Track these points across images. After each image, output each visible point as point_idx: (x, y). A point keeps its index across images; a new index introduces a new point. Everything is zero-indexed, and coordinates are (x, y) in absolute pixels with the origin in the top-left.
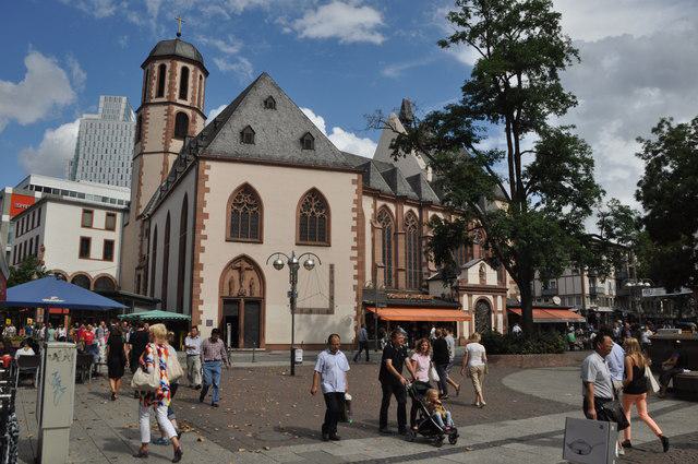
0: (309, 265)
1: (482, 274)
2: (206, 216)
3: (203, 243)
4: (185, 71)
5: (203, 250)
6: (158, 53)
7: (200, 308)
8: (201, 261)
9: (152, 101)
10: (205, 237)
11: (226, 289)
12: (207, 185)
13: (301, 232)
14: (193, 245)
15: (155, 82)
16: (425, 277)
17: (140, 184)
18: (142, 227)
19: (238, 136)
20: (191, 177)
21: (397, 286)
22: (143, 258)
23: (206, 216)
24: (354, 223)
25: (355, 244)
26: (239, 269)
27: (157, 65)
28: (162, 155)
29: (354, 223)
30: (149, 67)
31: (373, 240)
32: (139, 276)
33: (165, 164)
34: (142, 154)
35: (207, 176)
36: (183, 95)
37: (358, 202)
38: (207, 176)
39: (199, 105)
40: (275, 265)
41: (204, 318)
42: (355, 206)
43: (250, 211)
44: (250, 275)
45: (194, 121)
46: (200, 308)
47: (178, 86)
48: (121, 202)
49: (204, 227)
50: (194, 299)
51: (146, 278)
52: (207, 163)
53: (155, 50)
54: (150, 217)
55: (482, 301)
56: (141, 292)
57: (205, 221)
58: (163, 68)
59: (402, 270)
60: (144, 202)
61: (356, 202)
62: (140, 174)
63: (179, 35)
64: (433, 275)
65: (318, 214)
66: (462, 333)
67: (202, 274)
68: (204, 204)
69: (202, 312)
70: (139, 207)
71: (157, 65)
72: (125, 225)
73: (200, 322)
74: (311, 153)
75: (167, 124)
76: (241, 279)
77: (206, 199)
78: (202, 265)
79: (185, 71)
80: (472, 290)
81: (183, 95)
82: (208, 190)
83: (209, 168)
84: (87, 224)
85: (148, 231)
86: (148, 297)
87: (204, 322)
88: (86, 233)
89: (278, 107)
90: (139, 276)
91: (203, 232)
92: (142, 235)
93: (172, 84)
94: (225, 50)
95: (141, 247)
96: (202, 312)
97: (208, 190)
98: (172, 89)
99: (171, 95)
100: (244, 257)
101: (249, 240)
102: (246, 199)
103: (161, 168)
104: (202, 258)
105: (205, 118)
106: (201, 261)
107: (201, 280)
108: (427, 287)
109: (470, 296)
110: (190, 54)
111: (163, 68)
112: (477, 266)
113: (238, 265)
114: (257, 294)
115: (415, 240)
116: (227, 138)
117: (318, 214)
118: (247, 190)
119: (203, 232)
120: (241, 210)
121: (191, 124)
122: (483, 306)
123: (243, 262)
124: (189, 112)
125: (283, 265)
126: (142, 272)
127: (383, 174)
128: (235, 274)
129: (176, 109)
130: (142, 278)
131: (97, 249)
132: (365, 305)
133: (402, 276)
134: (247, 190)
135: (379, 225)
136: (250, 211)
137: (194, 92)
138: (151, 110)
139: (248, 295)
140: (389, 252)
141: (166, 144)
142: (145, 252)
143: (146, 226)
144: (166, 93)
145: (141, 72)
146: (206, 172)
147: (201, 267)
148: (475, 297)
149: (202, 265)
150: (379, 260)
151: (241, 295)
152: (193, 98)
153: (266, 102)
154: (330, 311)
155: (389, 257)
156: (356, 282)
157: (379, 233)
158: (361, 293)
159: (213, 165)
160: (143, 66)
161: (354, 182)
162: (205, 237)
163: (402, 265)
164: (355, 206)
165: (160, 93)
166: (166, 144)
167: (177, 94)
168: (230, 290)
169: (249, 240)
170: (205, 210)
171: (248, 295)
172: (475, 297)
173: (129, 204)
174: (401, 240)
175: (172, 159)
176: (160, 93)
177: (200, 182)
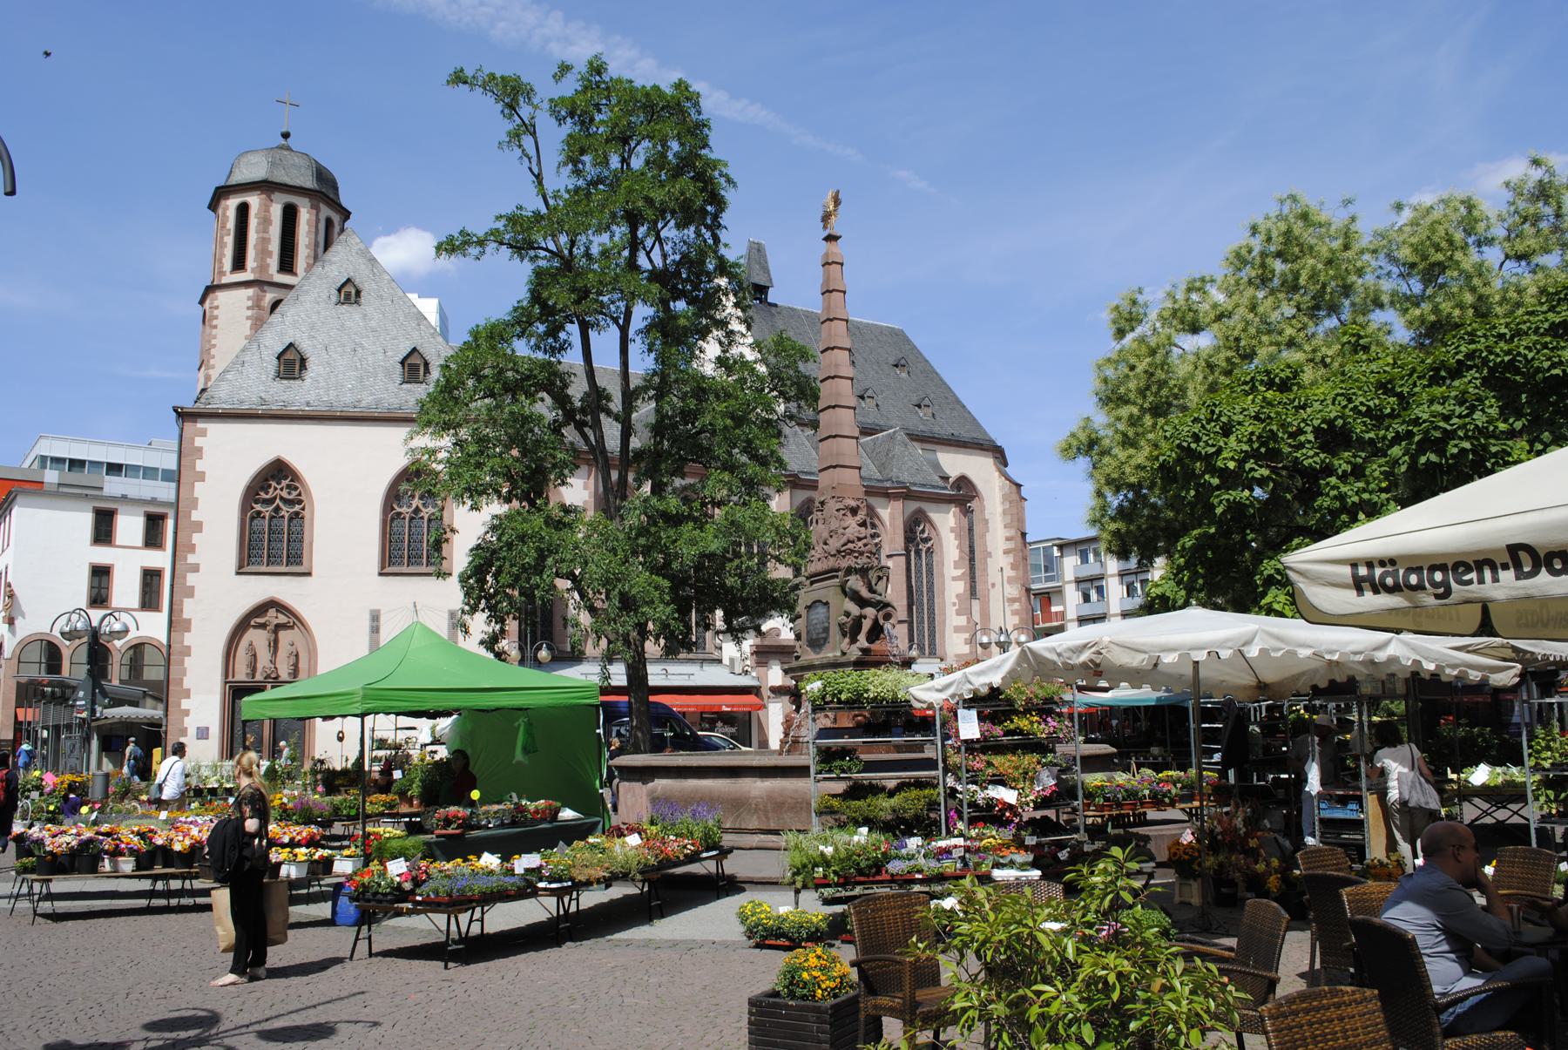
2: (198, 527)
5: (190, 592)
7: (185, 704)
8: (185, 615)
9: (225, 280)
10: (195, 568)
23: (198, 527)
27: (232, 203)
35: (200, 450)
38: (200, 450)
41: (191, 724)
43: (286, 511)
47: (275, 246)
49: (192, 548)
52: (200, 425)
57: (196, 538)
58: (243, 210)
68: (194, 503)
69: (187, 713)
71: (232, 203)
76: (274, 645)
78: (189, 622)
83: (203, 433)
84: (103, 530)
88: (102, 555)
91: (191, 559)
93: (264, 241)
96: (187, 713)
97: (201, 477)
98: (265, 222)
99: (263, 267)
100: (272, 604)
106: (185, 615)
107: (187, 651)
111: (243, 210)
117: (426, 512)
118: (278, 471)
119: (191, 559)
131: (125, 590)
134: (278, 471)
138: (222, 297)
146: (198, 442)
149: (189, 622)
159: (215, 429)
162: (195, 568)
165: (239, 263)
167: (274, 262)
169: (283, 569)
170: (195, 516)
176: (239, 263)
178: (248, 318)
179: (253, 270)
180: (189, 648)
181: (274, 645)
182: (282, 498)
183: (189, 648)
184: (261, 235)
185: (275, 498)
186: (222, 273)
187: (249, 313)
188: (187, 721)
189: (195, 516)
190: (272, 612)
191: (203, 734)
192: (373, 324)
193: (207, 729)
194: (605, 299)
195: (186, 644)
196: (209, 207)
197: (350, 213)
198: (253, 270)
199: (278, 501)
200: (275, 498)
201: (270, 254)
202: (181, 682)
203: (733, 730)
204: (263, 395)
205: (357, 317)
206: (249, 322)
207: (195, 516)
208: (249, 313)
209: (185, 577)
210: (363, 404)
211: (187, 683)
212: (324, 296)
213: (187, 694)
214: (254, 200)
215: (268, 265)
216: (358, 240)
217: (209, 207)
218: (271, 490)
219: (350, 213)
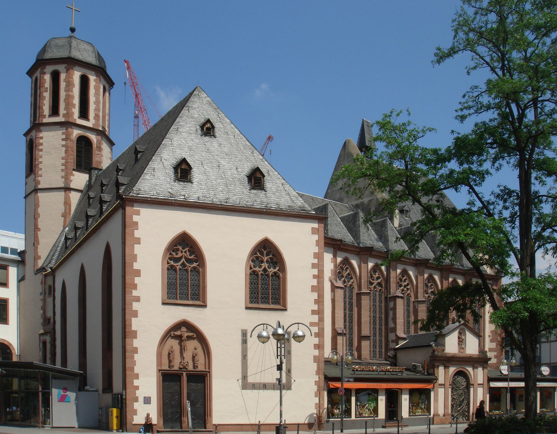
0: (299, 336)
1: (461, 341)
3: (136, 306)
4: (84, 81)
6: (48, 56)
7: (136, 383)
8: (134, 328)
9: (45, 120)
10: (138, 299)
11: (165, 361)
12: (137, 234)
13: (251, 293)
14: (124, 310)
15: (47, 96)
16: (392, 345)
17: (36, 228)
18: (44, 283)
19: (171, 172)
20: (116, 221)
21: (359, 357)
22: (47, 321)
24: (315, 282)
25: (316, 307)
26: (180, 338)
27: (50, 69)
28: (62, 194)
29: (315, 282)
30: (37, 74)
31: (333, 301)
32: (44, 343)
33: (67, 203)
34: (36, 190)
36: (84, 114)
37: (318, 256)
39: (103, 128)
40: (260, 337)
41: (140, 394)
42: (316, 261)
44: (192, 345)
45: (100, 149)
46: (136, 383)
47: (76, 101)
48: (14, 251)
49: (135, 287)
50: (128, 373)
51: (54, 346)
53: (44, 50)
54: (54, 271)
55: (460, 373)
56: (48, 361)
57: (137, 280)
59: (367, 338)
60: (44, 251)
61: (317, 256)
62: (36, 217)
63: (73, 30)
64: (401, 343)
65: (272, 270)
66: (436, 408)
67: (136, 343)
70: (37, 258)
72: (21, 279)
73: (136, 400)
74: (261, 194)
75: (66, 152)
76: (182, 350)
77: (136, 252)
78: (135, 332)
79: (84, 81)
80: (449, 361)
81: (84, 114)
82: (138, 241)
83: (138, 213)
85: (51, 290)
86: (58, 366)
87: (141, 400)
89: (217, 132)
90: (44, 343)
91: (135, 293)
92: (44, 293)
93: (69, 98)
94: (499, 9)
95: (44, 308)
96: (137, 388)
97: (138, 241)
99: (69, 114)
100: (185, 324)
101: (191, 302)
102: (183, 253)
103: (62, 208)
104: (135, 324)
105: (111, 143)
106: (134, 328)
107: (136, 350)
108: (395, 357)
109: (446, 367)
110: (91, 59)
112: (456, 334)
113: (178, 333)
114: (201, 368)
115: (380, 302)
116: (158, 174)
117: (272, 270)
120: (178, 265)
121: (95, 152)
122: (460, 379)
123: (184, 329)
124: (93, 138)
125: (268, 338)
126: (48, 339)
127: (342, 219)
128: (174, 344)
129: (76, 133)
130: (48, 346)
132: (328, 379)
133: (365, 344)
135: (340, 284)
136: (190, 266)
137: (97, 109)
139: (190, 367)
140: (351, 316)
141: (67, 178)
142: (50, 314)
143: (50, 281)
144: (62, 110)
145: (28, 81)
146: (135, 218)
147: (134, 335)
148: (452, 370)
149: (135, 332)
150: (340, 325)
151: (184, 368)
152: (97, 117)
153: (202, 127)
154: (246, 385)
155: (351, 322)
156: (316, 353)
157: (340, 293)
158: (322, 365)
160: (30, 73)
161: (314, 231)
162: (138, 299)
163: (366, 331)
164: (316, 261)
165: (55, 111)
166: (67, 178)
167: (76, 111)
168: (170, 361)
169: (191, 302)
171: (190, 367)
172: (452, 370)
173: (22, 254)
174: (366, 302)
175: (75, 197)
176: (55, 111)
177: (128, 230)
178: (63, 146)
179: (64, 115)
180: (136, 348)
181: (182, 350)
182: (185, 258)
183: (136, 348)
184: (70, 93)
185: (181, 258)
186: (44, 116)
187: (64, 143)
188: (138, 393)
189: (136, 266)
190: (184, 329)
191: (147, 401)
192: (226, 150)
193: (150, 398)
194: (474, 136)
195: (134, 346)
196: (28, 73)
197: (114, 84)
198: (64, 115)
199: (183, 260)
200: (181, 258)
201: (74, 106)
202: (133, 369)
203: (487, 408)
204: (170, 190)
205: (215, 144)
206: (64, 149)
207: (136, 266)
208: (64, 143)
209: (132, 305)
210: (231, 201)
211: (136, 370)
212: (193, 129)
213: (137, 376)
214: (61, 68)
215: (73, 113)
216: (205, 95)
217: (28, 73)
218: (179, 253)
219: (114, 84)
